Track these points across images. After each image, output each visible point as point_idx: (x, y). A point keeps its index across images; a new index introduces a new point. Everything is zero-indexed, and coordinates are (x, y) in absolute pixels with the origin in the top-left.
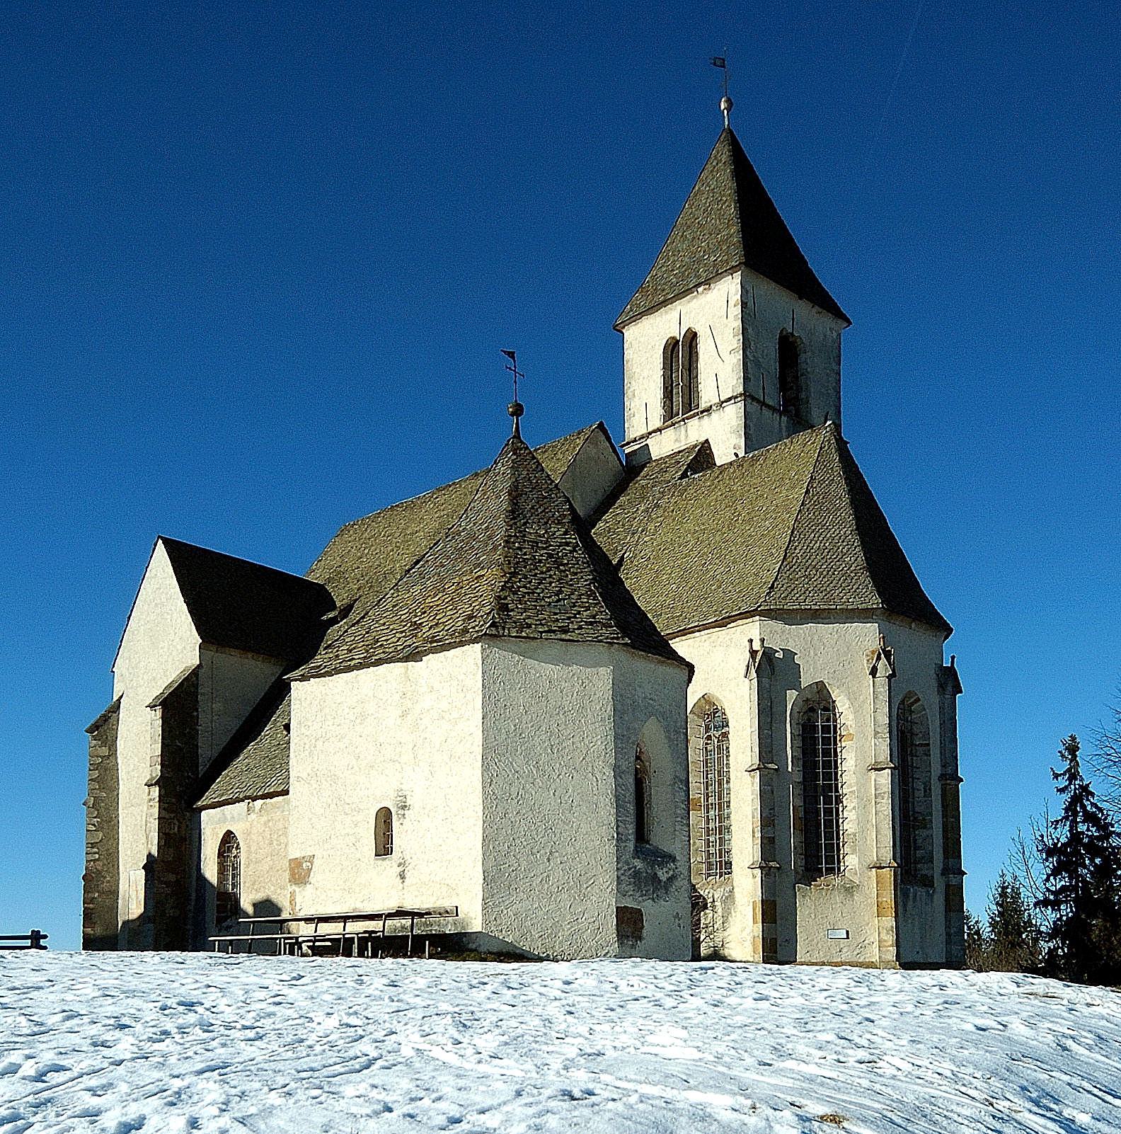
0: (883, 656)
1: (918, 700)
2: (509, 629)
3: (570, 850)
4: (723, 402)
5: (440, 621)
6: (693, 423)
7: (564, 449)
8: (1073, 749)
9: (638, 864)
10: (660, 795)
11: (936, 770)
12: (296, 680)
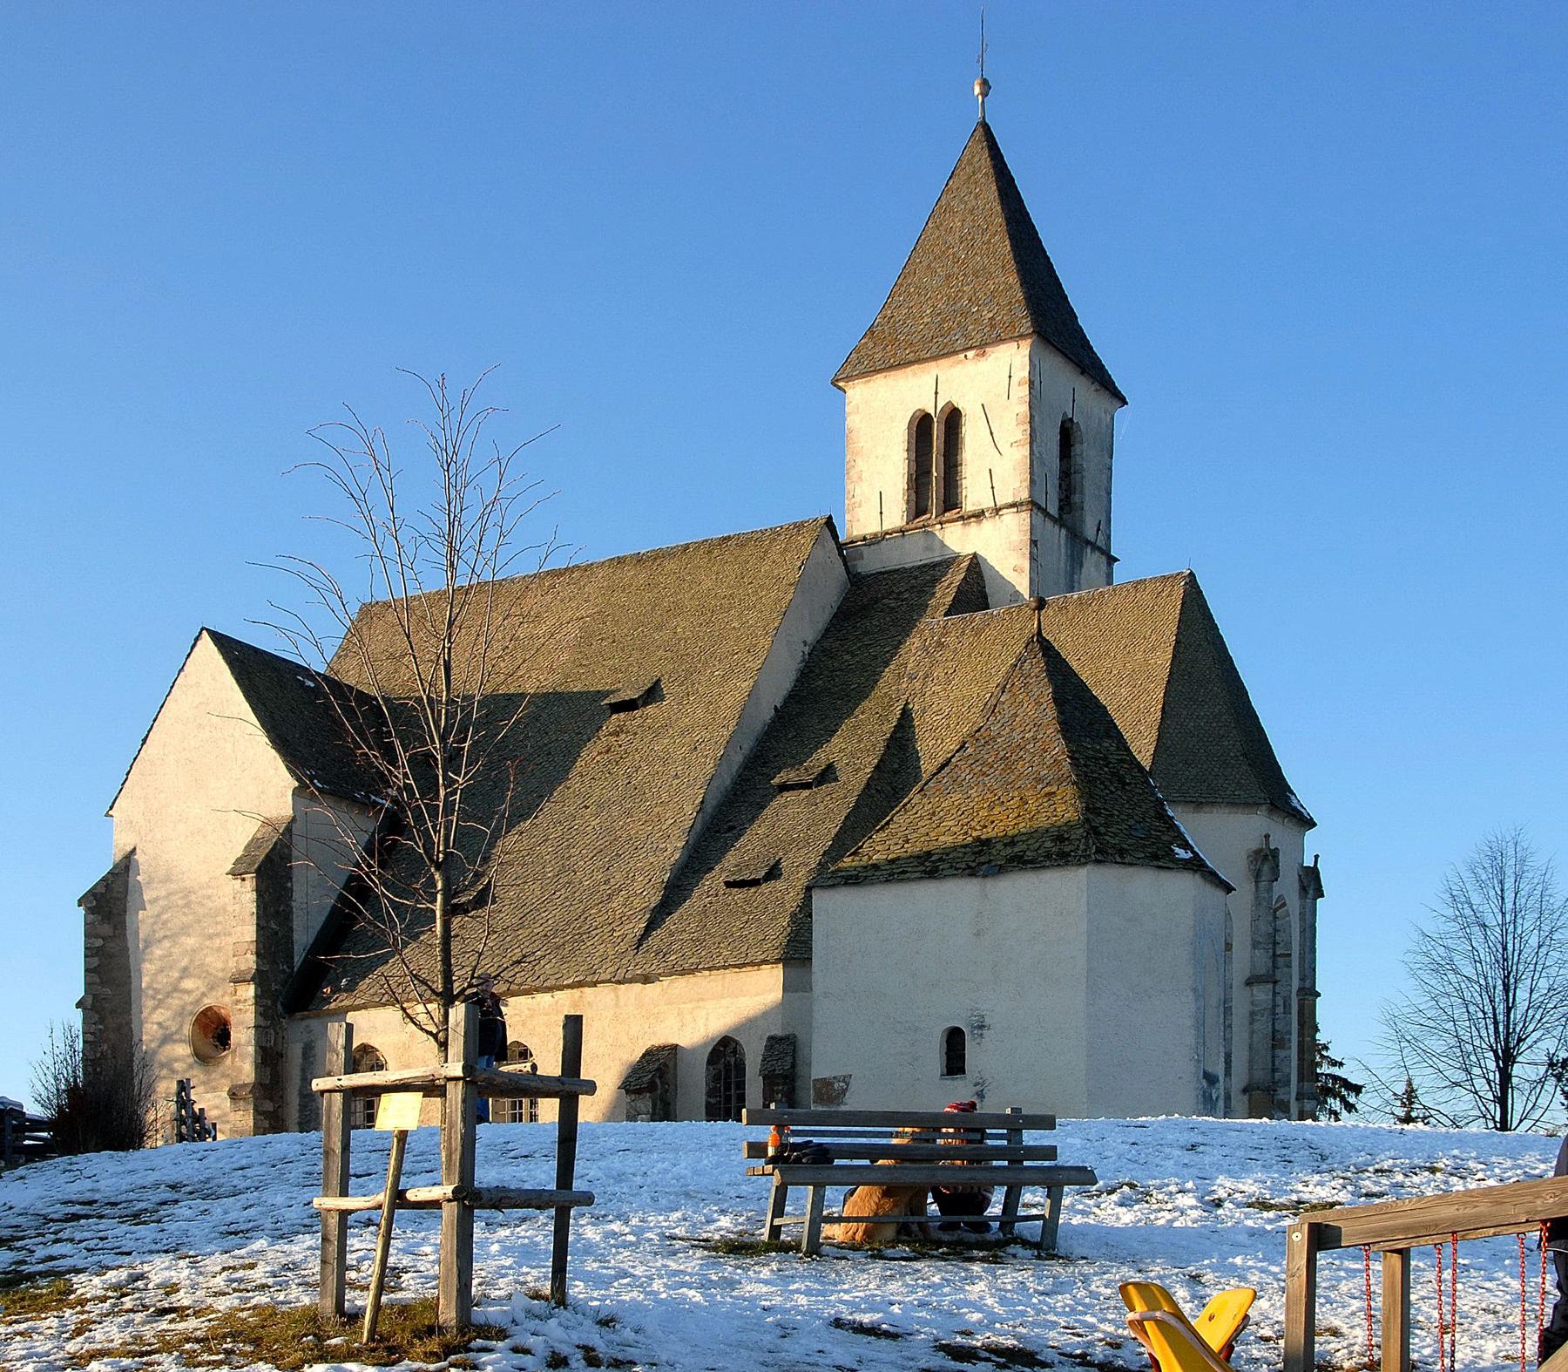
4: (1000, 509)
11: (1295, 984)
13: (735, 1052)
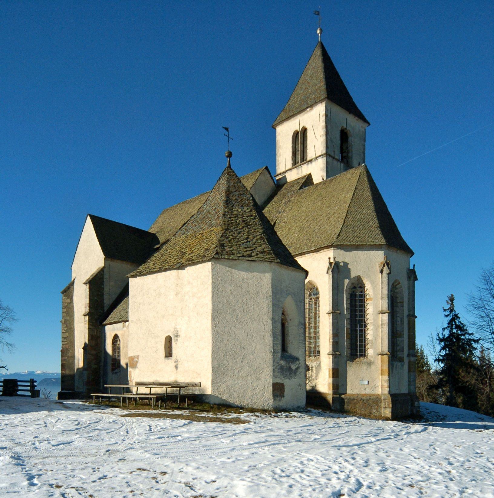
0: (386, 265)
1: (399, 283)
2: (224, 255)
3: (251, 357)
5: (194, 251)
6: (305, 167)
7: (251, 177)
8: (452, 299)
9: (283, 363)
10: (293, 331)
11: (406, 313)
12: (131, 277)
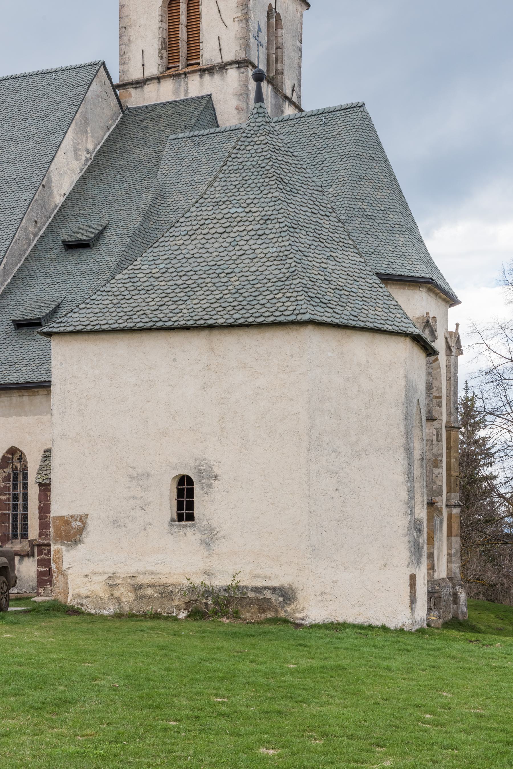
13: (20, 459)
